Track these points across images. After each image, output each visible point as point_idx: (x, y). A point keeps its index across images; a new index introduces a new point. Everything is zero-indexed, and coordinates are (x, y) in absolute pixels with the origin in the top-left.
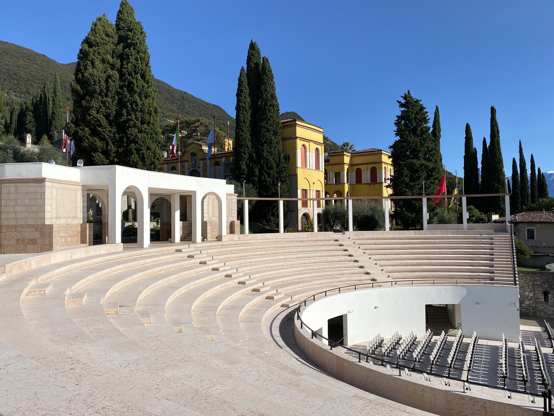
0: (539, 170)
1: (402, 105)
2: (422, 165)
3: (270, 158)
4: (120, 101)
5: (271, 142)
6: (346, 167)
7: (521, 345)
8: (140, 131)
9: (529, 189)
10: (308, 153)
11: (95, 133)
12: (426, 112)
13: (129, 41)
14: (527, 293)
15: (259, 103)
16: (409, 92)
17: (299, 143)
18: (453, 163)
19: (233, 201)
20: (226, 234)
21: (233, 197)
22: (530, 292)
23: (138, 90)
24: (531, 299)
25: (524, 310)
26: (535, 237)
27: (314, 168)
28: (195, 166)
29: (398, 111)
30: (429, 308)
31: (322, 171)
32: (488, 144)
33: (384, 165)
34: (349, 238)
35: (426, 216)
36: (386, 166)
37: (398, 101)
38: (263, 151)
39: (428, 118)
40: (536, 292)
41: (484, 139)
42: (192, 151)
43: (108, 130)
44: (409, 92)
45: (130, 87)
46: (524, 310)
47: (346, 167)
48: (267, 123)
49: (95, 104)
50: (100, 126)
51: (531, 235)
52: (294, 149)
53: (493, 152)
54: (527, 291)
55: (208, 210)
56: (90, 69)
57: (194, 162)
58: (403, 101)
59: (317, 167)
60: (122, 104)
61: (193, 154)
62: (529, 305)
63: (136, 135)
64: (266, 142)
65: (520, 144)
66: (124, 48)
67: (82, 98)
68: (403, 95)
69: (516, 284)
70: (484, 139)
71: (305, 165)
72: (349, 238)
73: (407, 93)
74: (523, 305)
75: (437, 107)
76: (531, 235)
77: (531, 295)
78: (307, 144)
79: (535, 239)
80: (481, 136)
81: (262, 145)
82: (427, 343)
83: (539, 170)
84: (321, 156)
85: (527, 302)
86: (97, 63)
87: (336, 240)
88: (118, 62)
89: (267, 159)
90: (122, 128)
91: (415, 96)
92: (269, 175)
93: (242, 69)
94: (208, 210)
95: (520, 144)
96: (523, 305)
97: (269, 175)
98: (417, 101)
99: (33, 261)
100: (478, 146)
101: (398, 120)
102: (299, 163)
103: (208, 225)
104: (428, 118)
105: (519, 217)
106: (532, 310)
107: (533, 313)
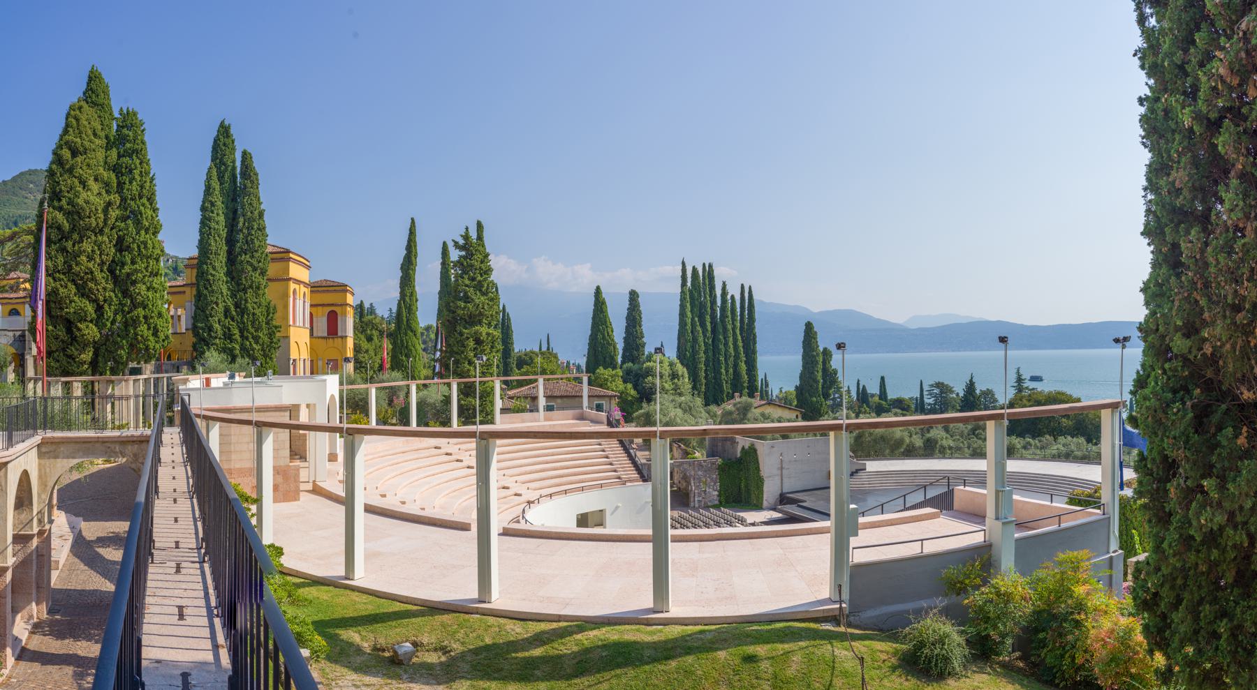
3: (257, 311)
4: (120, 240)
5: (258, 288)
11: (83, 292)
13: (128, 145)
31: (304, 327)
33: (292, 286)
36: (297, 287)
38: (246, 301)
43: (103, 285)
45: (136, 216)
48: (252, 257)
49: (87, 246)
50: (93, 279)
56: (84, 195)
58: (461, 242)
60: (121, 245)
64: (251, 287)
65: (412, 232)
66: (119, 156)
67: (65, 237)
73: (473, 235)
81: (245, 290)
86: (91, 182)
88: (113, 176)
89: (254, 314)
90: (123, 284)
92: (256, 339)
95: (412, 232)
97: (256, 339)
99: (316, 618)
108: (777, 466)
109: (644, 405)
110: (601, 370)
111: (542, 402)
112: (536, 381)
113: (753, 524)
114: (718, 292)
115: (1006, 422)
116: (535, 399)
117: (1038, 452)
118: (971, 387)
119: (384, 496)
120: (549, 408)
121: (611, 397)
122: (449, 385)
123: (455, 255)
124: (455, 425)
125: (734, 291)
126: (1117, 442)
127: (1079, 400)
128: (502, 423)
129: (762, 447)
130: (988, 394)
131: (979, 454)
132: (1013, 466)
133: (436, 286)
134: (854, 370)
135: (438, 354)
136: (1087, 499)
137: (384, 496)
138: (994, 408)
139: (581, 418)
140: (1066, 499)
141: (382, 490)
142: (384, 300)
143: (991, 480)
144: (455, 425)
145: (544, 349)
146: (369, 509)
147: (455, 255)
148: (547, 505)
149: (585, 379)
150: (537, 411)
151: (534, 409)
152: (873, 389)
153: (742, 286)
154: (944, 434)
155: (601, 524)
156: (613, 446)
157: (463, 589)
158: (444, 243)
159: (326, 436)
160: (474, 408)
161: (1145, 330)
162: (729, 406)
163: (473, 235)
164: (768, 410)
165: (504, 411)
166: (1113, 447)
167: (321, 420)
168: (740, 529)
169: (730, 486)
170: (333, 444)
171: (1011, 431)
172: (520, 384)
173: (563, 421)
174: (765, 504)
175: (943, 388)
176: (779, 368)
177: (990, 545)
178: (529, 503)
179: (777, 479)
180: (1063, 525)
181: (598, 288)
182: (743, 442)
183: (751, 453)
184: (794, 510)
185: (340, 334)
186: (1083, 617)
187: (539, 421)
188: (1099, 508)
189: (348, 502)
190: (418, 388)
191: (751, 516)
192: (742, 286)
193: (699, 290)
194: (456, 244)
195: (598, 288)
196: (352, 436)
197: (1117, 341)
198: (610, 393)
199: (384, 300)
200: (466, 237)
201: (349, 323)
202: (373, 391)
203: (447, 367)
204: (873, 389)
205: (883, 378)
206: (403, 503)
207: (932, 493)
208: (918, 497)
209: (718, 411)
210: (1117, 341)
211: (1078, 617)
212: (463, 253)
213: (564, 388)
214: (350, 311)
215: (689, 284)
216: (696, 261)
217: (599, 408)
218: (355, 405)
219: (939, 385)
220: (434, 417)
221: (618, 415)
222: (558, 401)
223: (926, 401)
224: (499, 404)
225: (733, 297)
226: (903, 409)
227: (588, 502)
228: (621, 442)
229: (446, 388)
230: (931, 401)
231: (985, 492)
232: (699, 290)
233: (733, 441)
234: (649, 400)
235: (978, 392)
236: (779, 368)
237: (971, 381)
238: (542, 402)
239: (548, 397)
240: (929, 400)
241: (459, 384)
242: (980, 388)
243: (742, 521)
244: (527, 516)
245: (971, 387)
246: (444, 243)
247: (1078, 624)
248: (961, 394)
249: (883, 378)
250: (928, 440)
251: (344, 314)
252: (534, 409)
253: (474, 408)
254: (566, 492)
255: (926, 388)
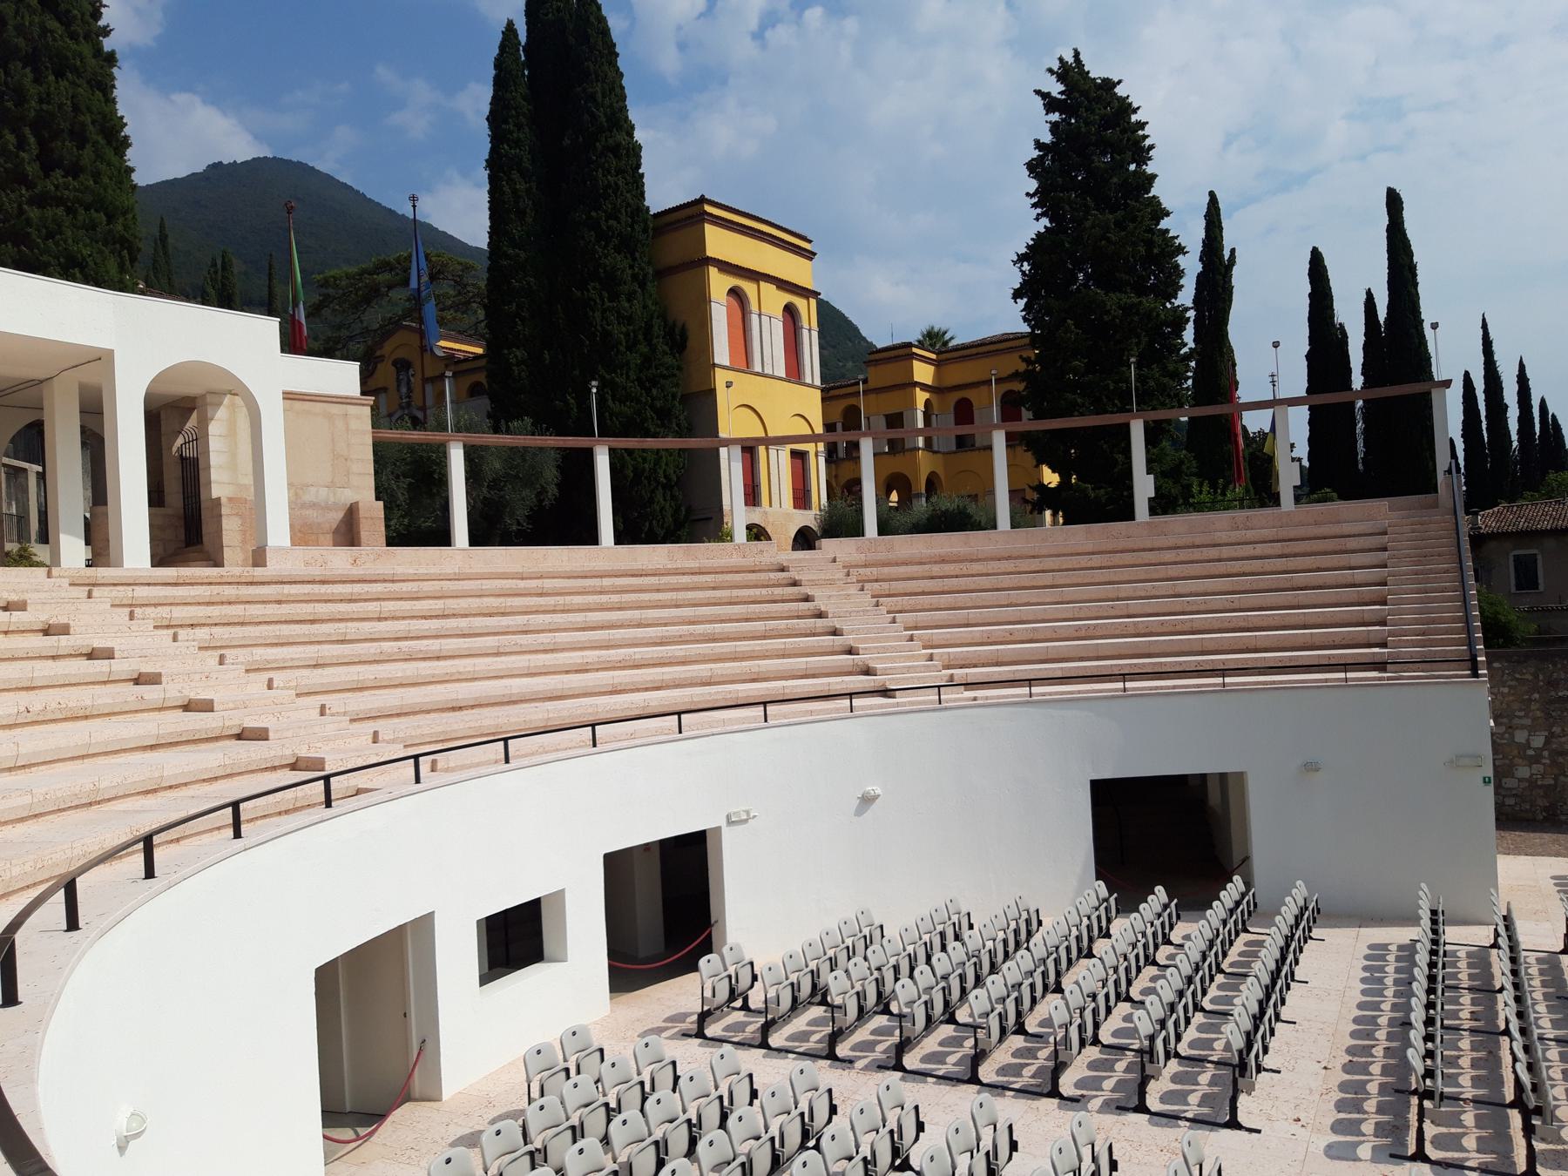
0: (1543, 402)
1: (1050, 104)
2: (1128, 310)
6: (921, 397)
7: (1502, 930)
8: (41, 201)
9: (1515, 451)
10: (755, 318)
12: (1142, 125)
14: (1521, 736)
15: (567, 142)
16: (1077, 54)
17: (719, 284)
18: (1268, 356)
19: (354, 425)
20: (286, 542)
21: (352, 410)
22: (1532, 730)
23: (21, 42)
24: (1537, 759)
25: (1511, 801)
26: (1541, 580)
27: (781, 371)
28: (409, 404)
29: (1039, 126)
30: (1104, 793)
32: (1382, 314)
34: (834, 561)
35: (1144, 486)
37: (1038, 92)
39: (1147, 142)
40: (1557, 730)
41: (1369, 294)
42: (401, 354)
44: (1077, 54)
46: (1511, 801)
47: (921, 397)
51: (1526, 576)
52: (704, 300)
53: (1400, 334)
54: (1523, 727)
55: (233, 455)
57: (404, 390)
58: (1056, 89)
59: (794, 372)
61: (403, 366)
62: (1531, 783)
63: (21, 212)
65: (1485, 326)
68: (1056, 66)
69: (1476, 675)
70: (1369, 294)
71: (744, 359)
72: (834, 561)
73: (1070, 59)
74: (1509, 783)
75: (1212, 194)
76: (1526, 576)
77: (1538, 741)
78: (749, 288)
79: (1541, 588)
80: (1359, 280)
82: (1211, 959)
83: (1543, 402)
84: (805, 333)
85: (1523, 772)
87: (783, 570)
91: (1097, 70)
93: (510, 29)
94: (233, 455)
95: (1485, 326)
96: (1509, 783)
98: (1109, 85)
100: (1349, 316)
101: (1040, 159)
102: (721, 352)
103: (224, 511)
104: (1147, 142)
105: (1488, 520)
106: (1540, 802)
107: (1545, 809)
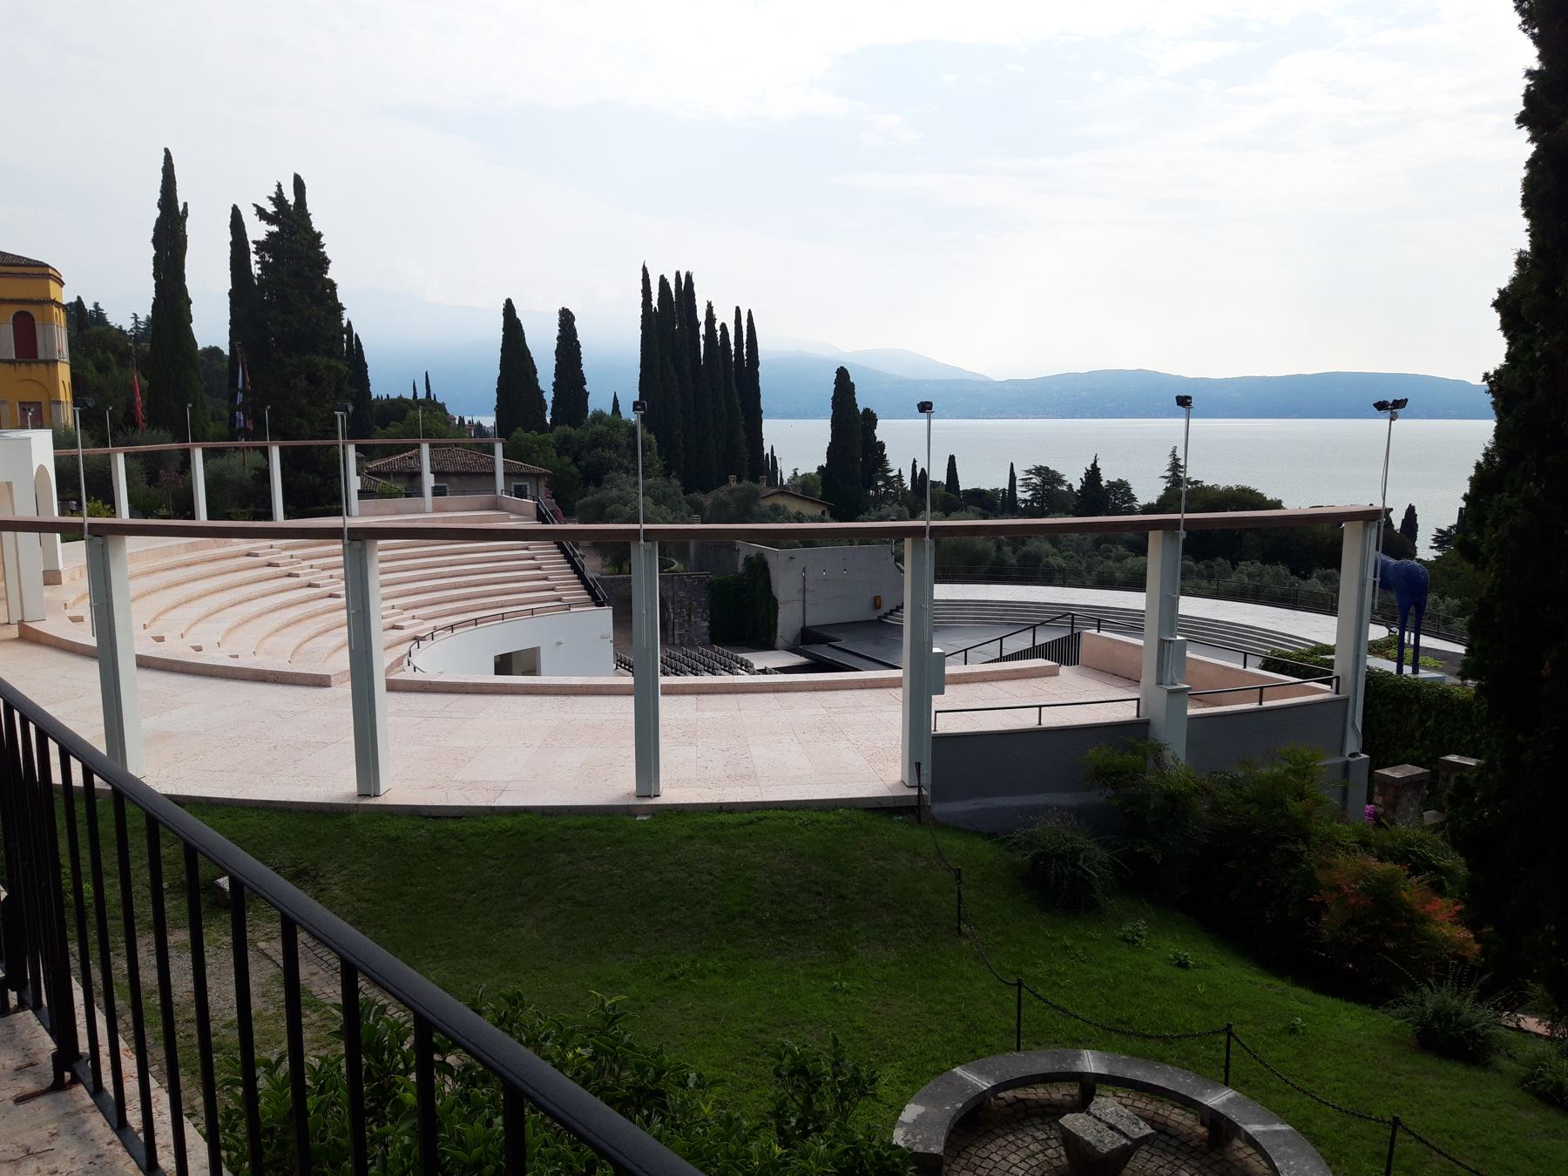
58: (270, 208)
73: (290, 197)
108: (800, 587)
109: (591, 489)
110: (519, 433)
111: (429, 481)
112: (418, 446)
113: (764, 671)
114: (701, 316)
115: (1182, 534)
116: (416, 475)
117: (1204, 583)
118: (1093, 474)
119: (160, 639)
120: (437, 492)
121: (538, 476)
122: (265, 452)
123: (257, 231)
124: (280, 520)
125: (724, 317)
126: (1370, 575)
127: (1277, 505)
128: (359, 515)
129: (776, 558)
130: (1121, 487)
131: (1136, 582)
132: (1190, 606)
133: (223, 282)
134: (904, 446)
135: (240, 396)
136: (1306, 663)
137: (160, 639)
138: (1131, 511)
139: (495, 506)
140: (1259, 661)
141: (155, 630)
142: (127, 300)
143: (1152, 625)
144: (280, 520)
145: (422, 395)
146: (144, 663)
147: (257, 231)
148: (445, 641)
149: (499, 448)
150: (420, 494)
151: (415, 491)
152: (939, 474)
153: (738, 310)
154: (1047, 546)
155: (533, 671)
156: (545, 552)
157: (328, 779)
158: (235, 209)
159: (29, 539)
160: (315, 493)
161: (1498, 383)
162: (721, 493)
163: (290, 197)
164: (782, 501)
165: (363, 494)
166: (1362, 585)
167: (26, 512)
168: (744, 678)
169: (727, 622)
170: (51, 555)
171: (1190, 549)
172: (388, 451)
173: (461, 513)
174: (779, 642)
175: (1048, 477)
176: (797, 443)
177: (1147, 723)
178: (417, 639)
179: (798, 606)
180: (1266, 704)
181: (509, 302)
182: (747, 549)
183: (759, 567)
184: (823, 651)
185: (41, 356)
186: (1302, 847)
187: (426, 511)
188: (1328, 682)
189: (105, 654)
190: (207, 454)
191: (759, 660)
192: (738, 310)
193: (670, 315)
194: (261, 213)
195: (509, 302)
196: (101, 538)
197: (1381, 406)
198: (537, 469)
199: (127, 300)
200: (279, 200)
201: (60, 338)
202: (121, 459)
203: (259, 422)
204: (939, 474)
205: (952, 458)
206: (199, 649)
207: (1043, 638)
208: (1023, 642)
209: (707, 500)
210: (1381, 406)
211: (1293, 847)
212: (275, 228)
213: (460, 459)
214: (60, 317)
215: (655, 303)
216: (665, 268)
217: (520, 492)
218: (80, 484)
219: (1041, 471)
220: (240, 505)
221: (549, 505)
222: (448, 481)
223: (1020, 495)
224: (355, 483)
225: (723, 326)
226: (983, 507)
227: (512, 638)
228: (561, 547)
229: (259, 456)
230: (1027, 496)
231: (1140, 642)
232: (670, 315)
233: (733, 549)
234: (598, 483)
235: (1104, 483)
236: (797, 443)
237: (1094, 466)
238: (429, 481)
239: (438, 474)
240: (1023, 494)
241: (282, 449)
242: (1108, 476)
243: (747, 667)
244: (415, 660)
245: (1093, 474)
246: (235, 209)
247: (1295, 858)
248: (1077, 486)
249: (952, 458)
250: (1026, 556)
251: (49, 322)
252: (415, 491)
253: (315, 493)
254: (476, 622)
255: (1019, 475)
